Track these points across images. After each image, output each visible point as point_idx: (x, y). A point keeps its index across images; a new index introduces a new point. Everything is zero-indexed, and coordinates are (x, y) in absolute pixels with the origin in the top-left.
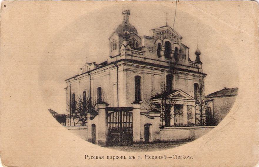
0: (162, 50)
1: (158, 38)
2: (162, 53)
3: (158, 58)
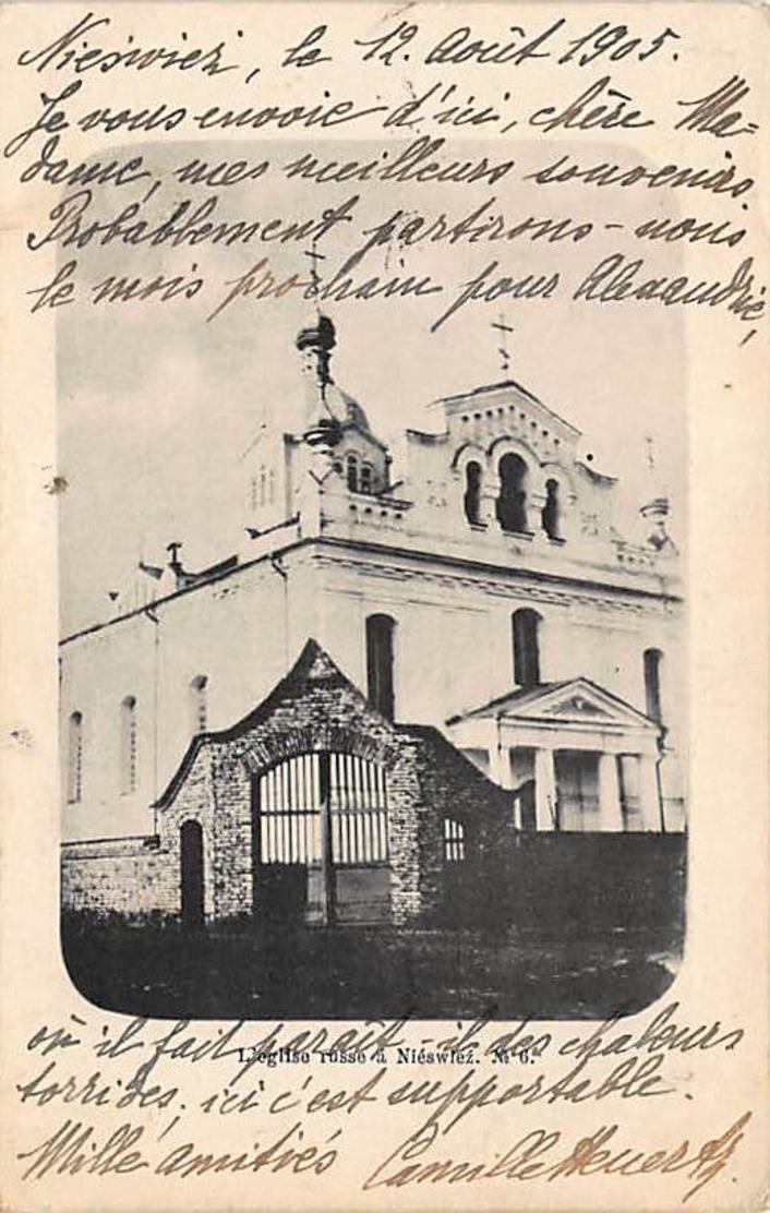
2: (487, 509)
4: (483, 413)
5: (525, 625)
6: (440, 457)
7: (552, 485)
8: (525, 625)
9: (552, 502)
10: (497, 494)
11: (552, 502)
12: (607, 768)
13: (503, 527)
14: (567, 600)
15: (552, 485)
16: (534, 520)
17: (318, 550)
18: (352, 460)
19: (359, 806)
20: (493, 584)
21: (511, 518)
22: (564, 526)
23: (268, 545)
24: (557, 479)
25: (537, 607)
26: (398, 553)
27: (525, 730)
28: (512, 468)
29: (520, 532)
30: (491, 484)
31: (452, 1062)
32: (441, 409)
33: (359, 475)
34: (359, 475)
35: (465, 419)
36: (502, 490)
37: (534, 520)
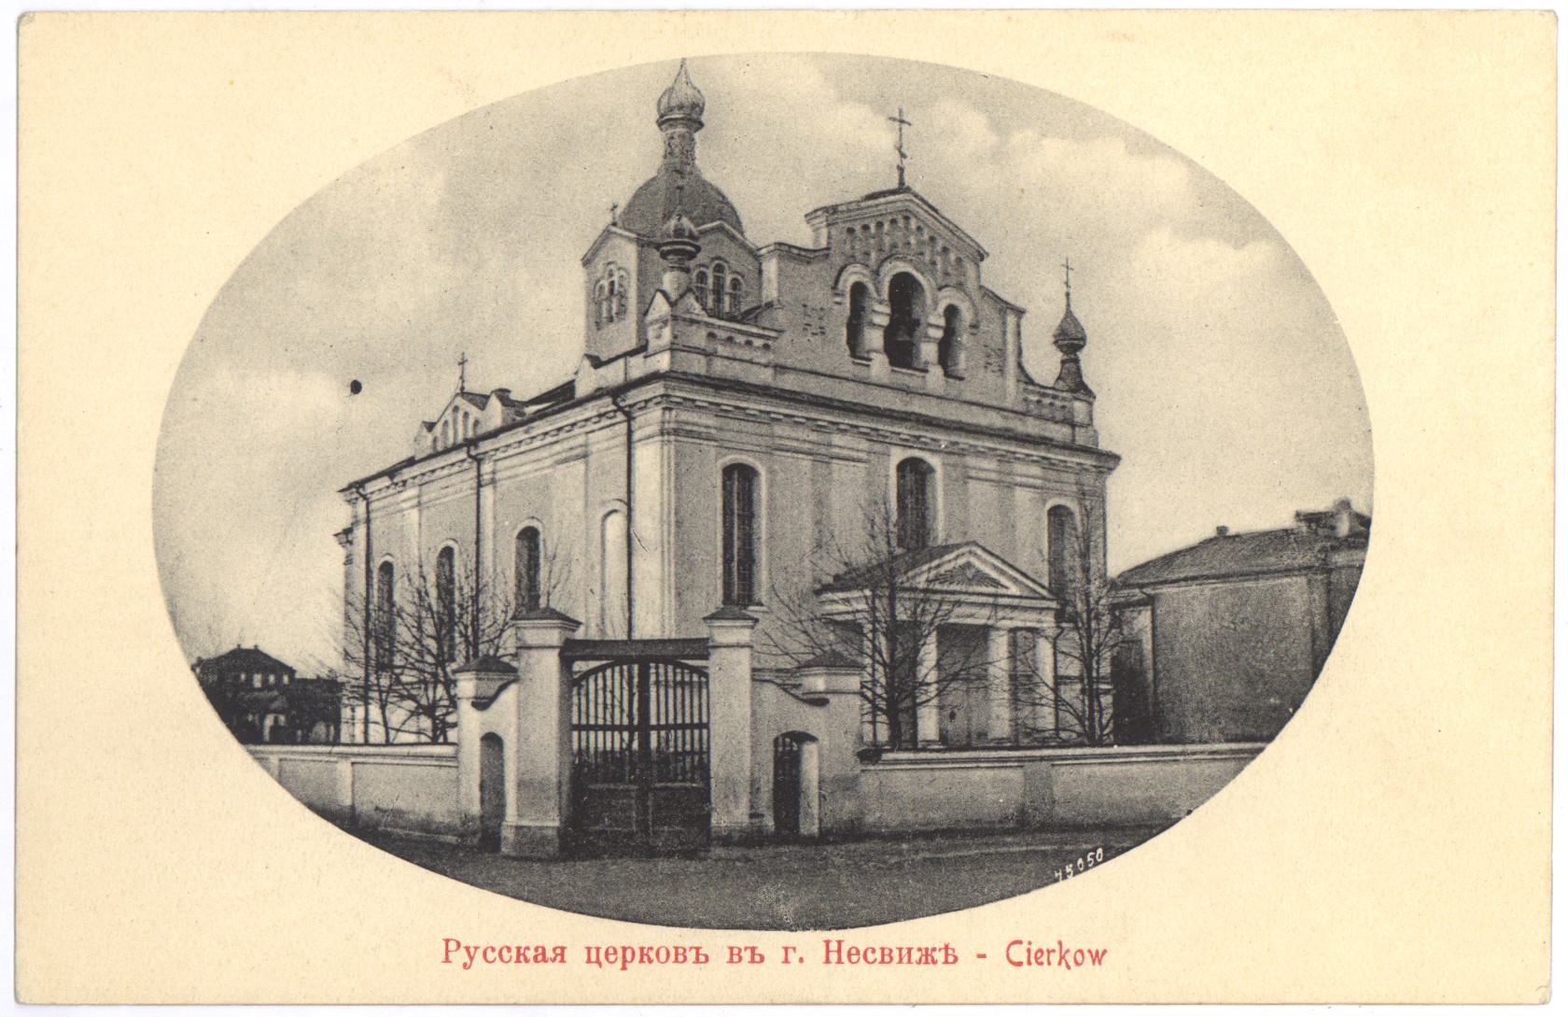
0: (873, 325)
1: (851, 259)
2: (874, 338)
3: (847, 366)
4: (858, 228)
5: (914, 473)
6: (816, 275)
7: (951, 312)
8: (914, 473)
9: (950, 331)
10: (885, 321)
11: (950, 331)
12: (999, 647)
13: (892, 363)
14: (963, 449)
15: (951, 312)
16: (929, 351)
17: (666, 387)
18: (719, 269)
19: (696, 690)
20: (876, 430)
21: (901, 351)
22: (963, 361)
23: (613, 375)
24: (955, 302)
25: (927, 457)
26: (764, 391)
27: (712, 711)
28: (904, 290)
29: (909, 366)
30: (880, 314)
31: (839, 961)
32: (821, 220)
33: (728, 289)
34: (728, 289)
35: (851, 231)
36: (892, 316)
37: (929, 351)
